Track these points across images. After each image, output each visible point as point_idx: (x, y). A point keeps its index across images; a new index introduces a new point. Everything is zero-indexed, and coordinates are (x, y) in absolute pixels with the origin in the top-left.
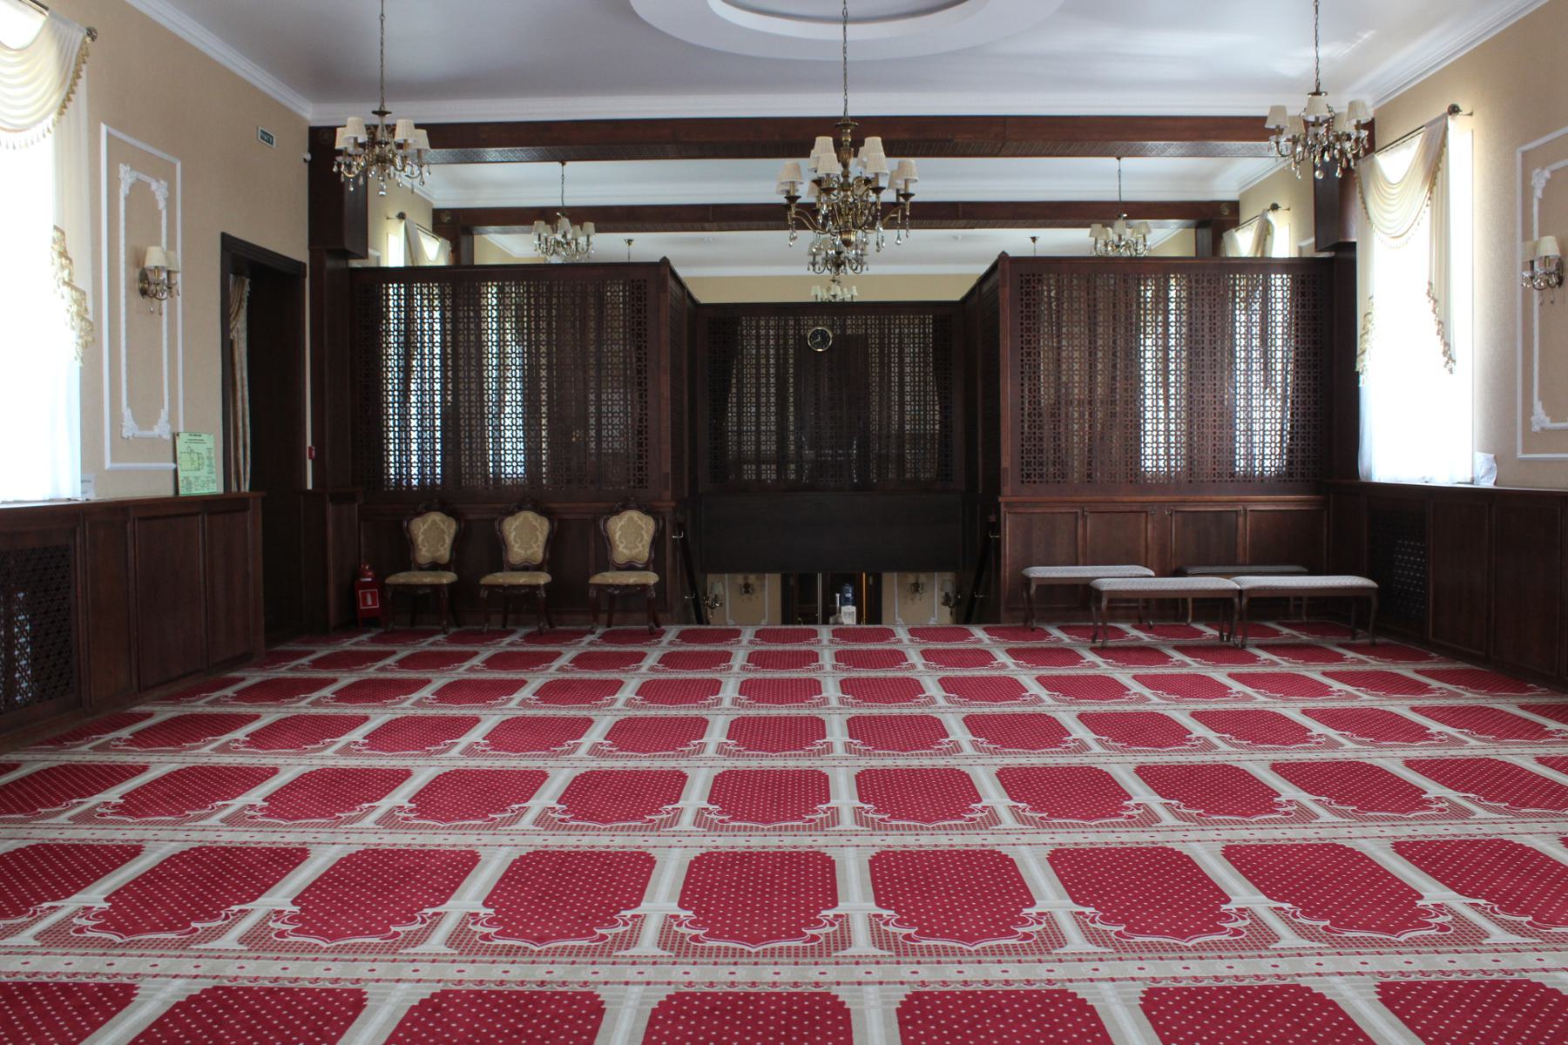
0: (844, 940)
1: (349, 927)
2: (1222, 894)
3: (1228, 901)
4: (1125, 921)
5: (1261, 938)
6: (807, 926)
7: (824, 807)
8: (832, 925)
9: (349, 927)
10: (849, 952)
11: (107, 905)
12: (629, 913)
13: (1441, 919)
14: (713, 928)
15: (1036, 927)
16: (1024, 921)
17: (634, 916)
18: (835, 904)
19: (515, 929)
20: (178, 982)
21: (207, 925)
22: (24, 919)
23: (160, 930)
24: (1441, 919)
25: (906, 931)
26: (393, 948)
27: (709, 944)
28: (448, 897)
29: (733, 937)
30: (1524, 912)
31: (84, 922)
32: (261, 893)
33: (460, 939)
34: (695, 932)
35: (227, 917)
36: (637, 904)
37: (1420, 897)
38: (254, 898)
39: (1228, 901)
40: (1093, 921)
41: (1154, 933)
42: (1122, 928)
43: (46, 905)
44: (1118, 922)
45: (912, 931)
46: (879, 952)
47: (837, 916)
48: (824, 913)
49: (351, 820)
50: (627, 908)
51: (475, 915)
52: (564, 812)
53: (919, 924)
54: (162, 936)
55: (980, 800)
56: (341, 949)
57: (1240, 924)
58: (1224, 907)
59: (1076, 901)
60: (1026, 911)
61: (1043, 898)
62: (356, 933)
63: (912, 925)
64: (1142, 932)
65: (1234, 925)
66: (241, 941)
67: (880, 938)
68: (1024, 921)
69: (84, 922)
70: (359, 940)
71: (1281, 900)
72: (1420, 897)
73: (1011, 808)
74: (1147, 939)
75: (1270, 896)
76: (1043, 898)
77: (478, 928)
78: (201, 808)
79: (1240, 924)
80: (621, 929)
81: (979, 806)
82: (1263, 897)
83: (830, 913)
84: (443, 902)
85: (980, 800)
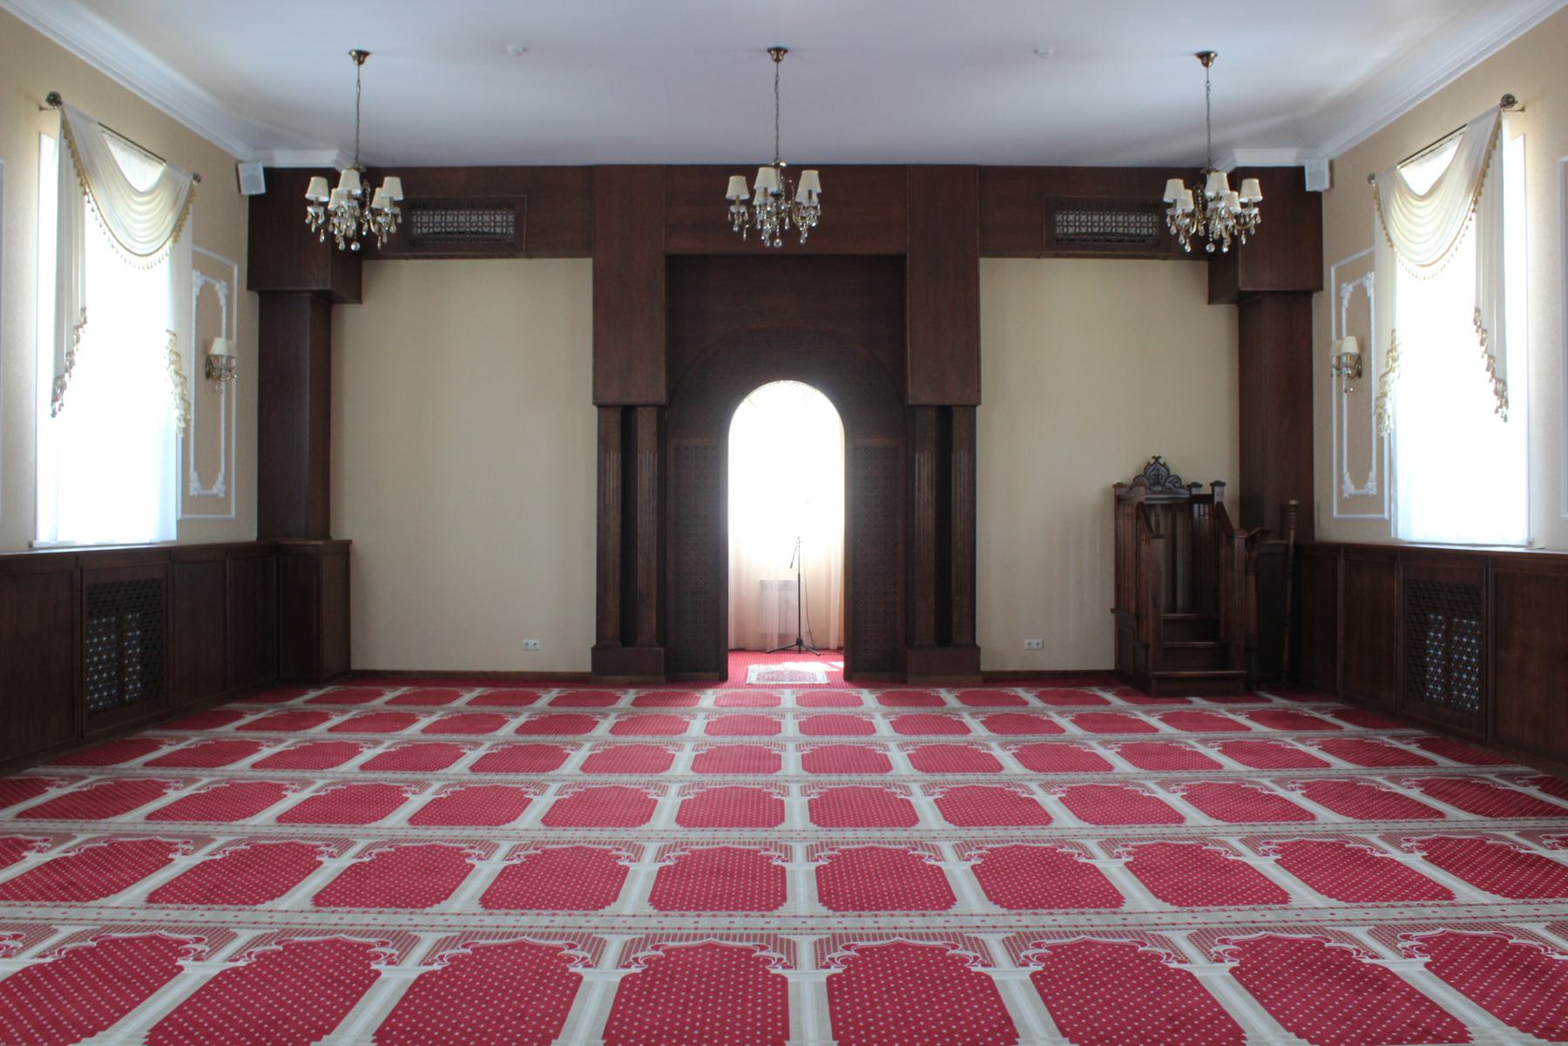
0: (822, 950)
1: (322, 949)
2: (1238, 978)
3: (1233, 971)
4: (1138, 956)
5: (1201, 938)
6: (856, 959)
7: (821, 863)
8: (832, 959)
9: (322, 949)
10: (816, 938)
11: (180, 962)
12: (634, 970)
13: (1408, 944)
14: (748, 957)
15: (1030, 953)
16: (1041, 958)
17: (628, 966)
18: (829, 980)
19: (546, 952)
20: (283, 908)
21: (83, 944)
22: (70, 946)
23: (125, 940)
24: (1408, 944)
25: (764, 953)
26: (466, 937)
27: (750, 944)
28: (416, 983)
29: (730, 949)
30: (1516, 947)
31: (12, 944)
32: (214, 980)
33: (406, 941)
34: (764, 953)
35: (249, 955)
36: (624, 980)
37: (1427, 965)
38: (222, 974)
39: (1233, 971)
40: (1169, 955)
41: (1112, 945)
42: (1140, 949)
43: (49, 960)
44: (1145, 953)
45: (951, 952)
46: (792, 938)
47: (828, 967)
48: (839, 971)
49: (238, 842)
50: (635, 975)
51: (587, 966)
52: (469, 855)
53: (945, 959)
54: (126, 935)
55: (973, 867)
56: (149, 928)
57: (1221, 948)
58: (1236, 964)
59: (989, 979)
60: (1039, 968)
61: (1023, 983)
62: (315, 944)
63: (952, 957)
64: (1122, 946)
65: (1226, 947)
66: (234, 936)
67: (789, 948)
68: (1041, 958)
69: (12, 944)
70: (313, 939)
71: (1178, 971)
72: (1427, 965)
73: (942, 859)
74: (1118, 940)
75: (1190, 975)
76: (1023, 983)
77: (581, 954)
78: (235, 852)
79: (1221, 948)
80: (640, 955)
81: (973, 862)
82: (1197, 974)
83: (834, 970)
84: (421, 977)
85: (973, 867)
